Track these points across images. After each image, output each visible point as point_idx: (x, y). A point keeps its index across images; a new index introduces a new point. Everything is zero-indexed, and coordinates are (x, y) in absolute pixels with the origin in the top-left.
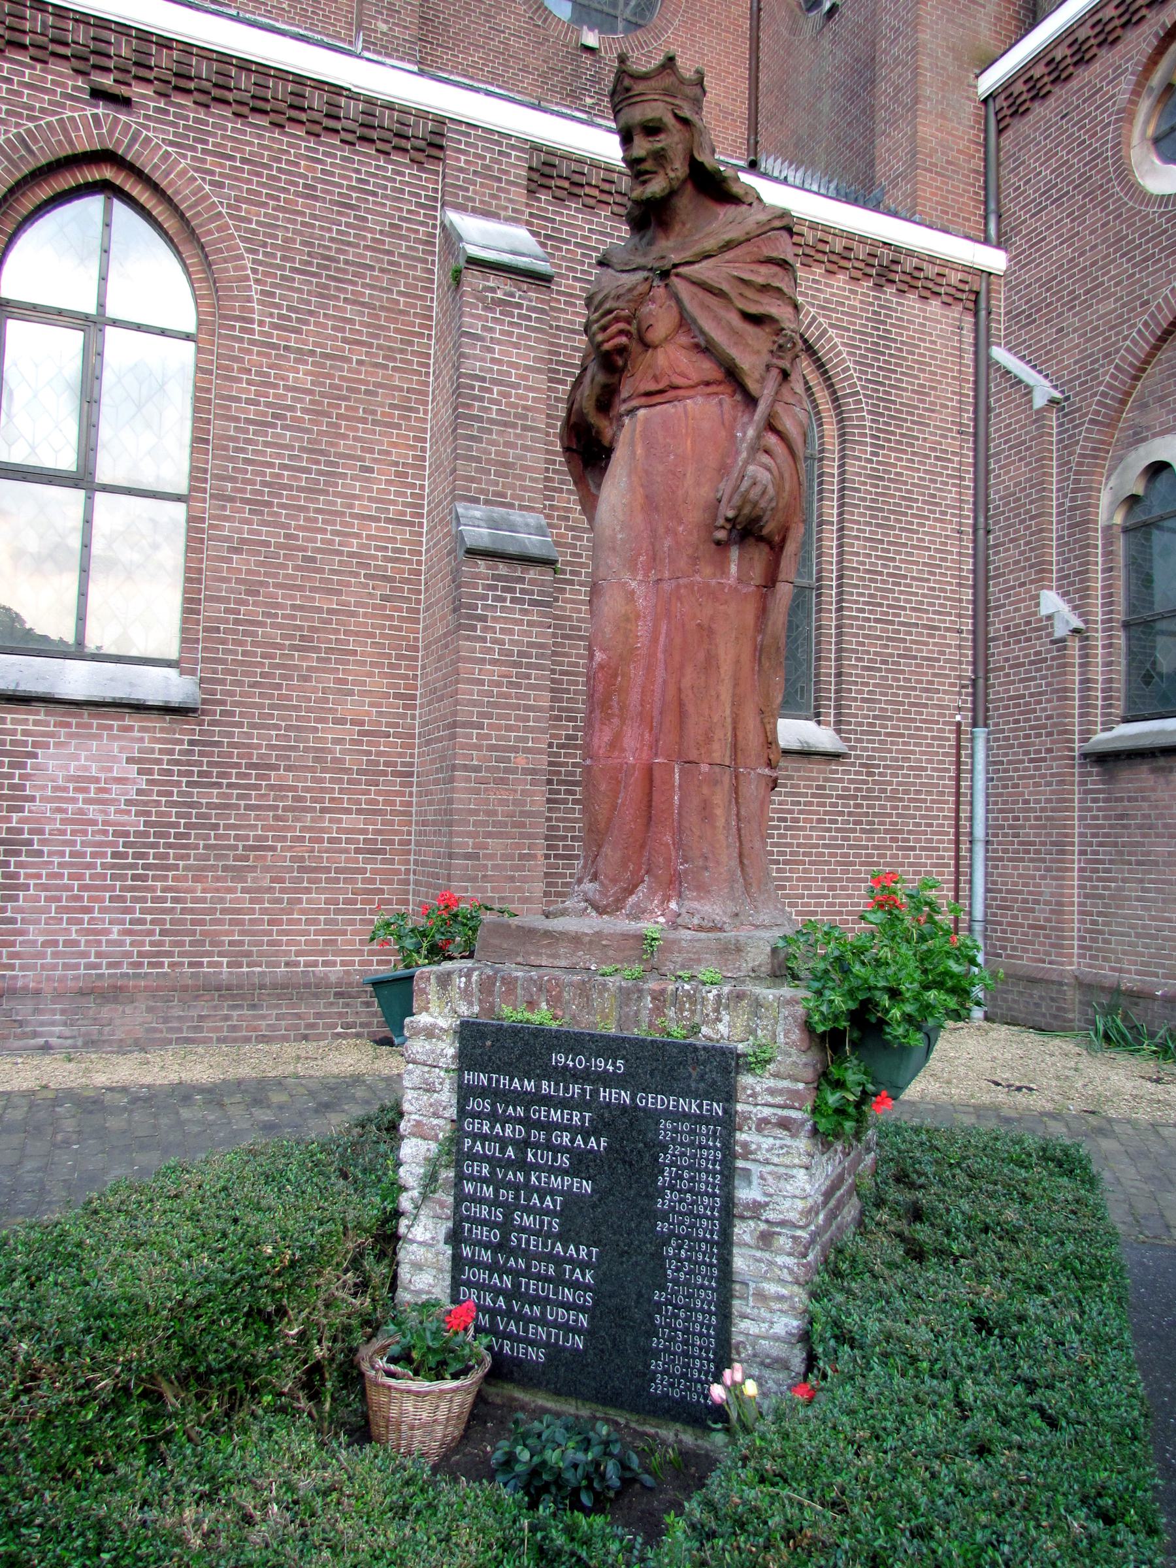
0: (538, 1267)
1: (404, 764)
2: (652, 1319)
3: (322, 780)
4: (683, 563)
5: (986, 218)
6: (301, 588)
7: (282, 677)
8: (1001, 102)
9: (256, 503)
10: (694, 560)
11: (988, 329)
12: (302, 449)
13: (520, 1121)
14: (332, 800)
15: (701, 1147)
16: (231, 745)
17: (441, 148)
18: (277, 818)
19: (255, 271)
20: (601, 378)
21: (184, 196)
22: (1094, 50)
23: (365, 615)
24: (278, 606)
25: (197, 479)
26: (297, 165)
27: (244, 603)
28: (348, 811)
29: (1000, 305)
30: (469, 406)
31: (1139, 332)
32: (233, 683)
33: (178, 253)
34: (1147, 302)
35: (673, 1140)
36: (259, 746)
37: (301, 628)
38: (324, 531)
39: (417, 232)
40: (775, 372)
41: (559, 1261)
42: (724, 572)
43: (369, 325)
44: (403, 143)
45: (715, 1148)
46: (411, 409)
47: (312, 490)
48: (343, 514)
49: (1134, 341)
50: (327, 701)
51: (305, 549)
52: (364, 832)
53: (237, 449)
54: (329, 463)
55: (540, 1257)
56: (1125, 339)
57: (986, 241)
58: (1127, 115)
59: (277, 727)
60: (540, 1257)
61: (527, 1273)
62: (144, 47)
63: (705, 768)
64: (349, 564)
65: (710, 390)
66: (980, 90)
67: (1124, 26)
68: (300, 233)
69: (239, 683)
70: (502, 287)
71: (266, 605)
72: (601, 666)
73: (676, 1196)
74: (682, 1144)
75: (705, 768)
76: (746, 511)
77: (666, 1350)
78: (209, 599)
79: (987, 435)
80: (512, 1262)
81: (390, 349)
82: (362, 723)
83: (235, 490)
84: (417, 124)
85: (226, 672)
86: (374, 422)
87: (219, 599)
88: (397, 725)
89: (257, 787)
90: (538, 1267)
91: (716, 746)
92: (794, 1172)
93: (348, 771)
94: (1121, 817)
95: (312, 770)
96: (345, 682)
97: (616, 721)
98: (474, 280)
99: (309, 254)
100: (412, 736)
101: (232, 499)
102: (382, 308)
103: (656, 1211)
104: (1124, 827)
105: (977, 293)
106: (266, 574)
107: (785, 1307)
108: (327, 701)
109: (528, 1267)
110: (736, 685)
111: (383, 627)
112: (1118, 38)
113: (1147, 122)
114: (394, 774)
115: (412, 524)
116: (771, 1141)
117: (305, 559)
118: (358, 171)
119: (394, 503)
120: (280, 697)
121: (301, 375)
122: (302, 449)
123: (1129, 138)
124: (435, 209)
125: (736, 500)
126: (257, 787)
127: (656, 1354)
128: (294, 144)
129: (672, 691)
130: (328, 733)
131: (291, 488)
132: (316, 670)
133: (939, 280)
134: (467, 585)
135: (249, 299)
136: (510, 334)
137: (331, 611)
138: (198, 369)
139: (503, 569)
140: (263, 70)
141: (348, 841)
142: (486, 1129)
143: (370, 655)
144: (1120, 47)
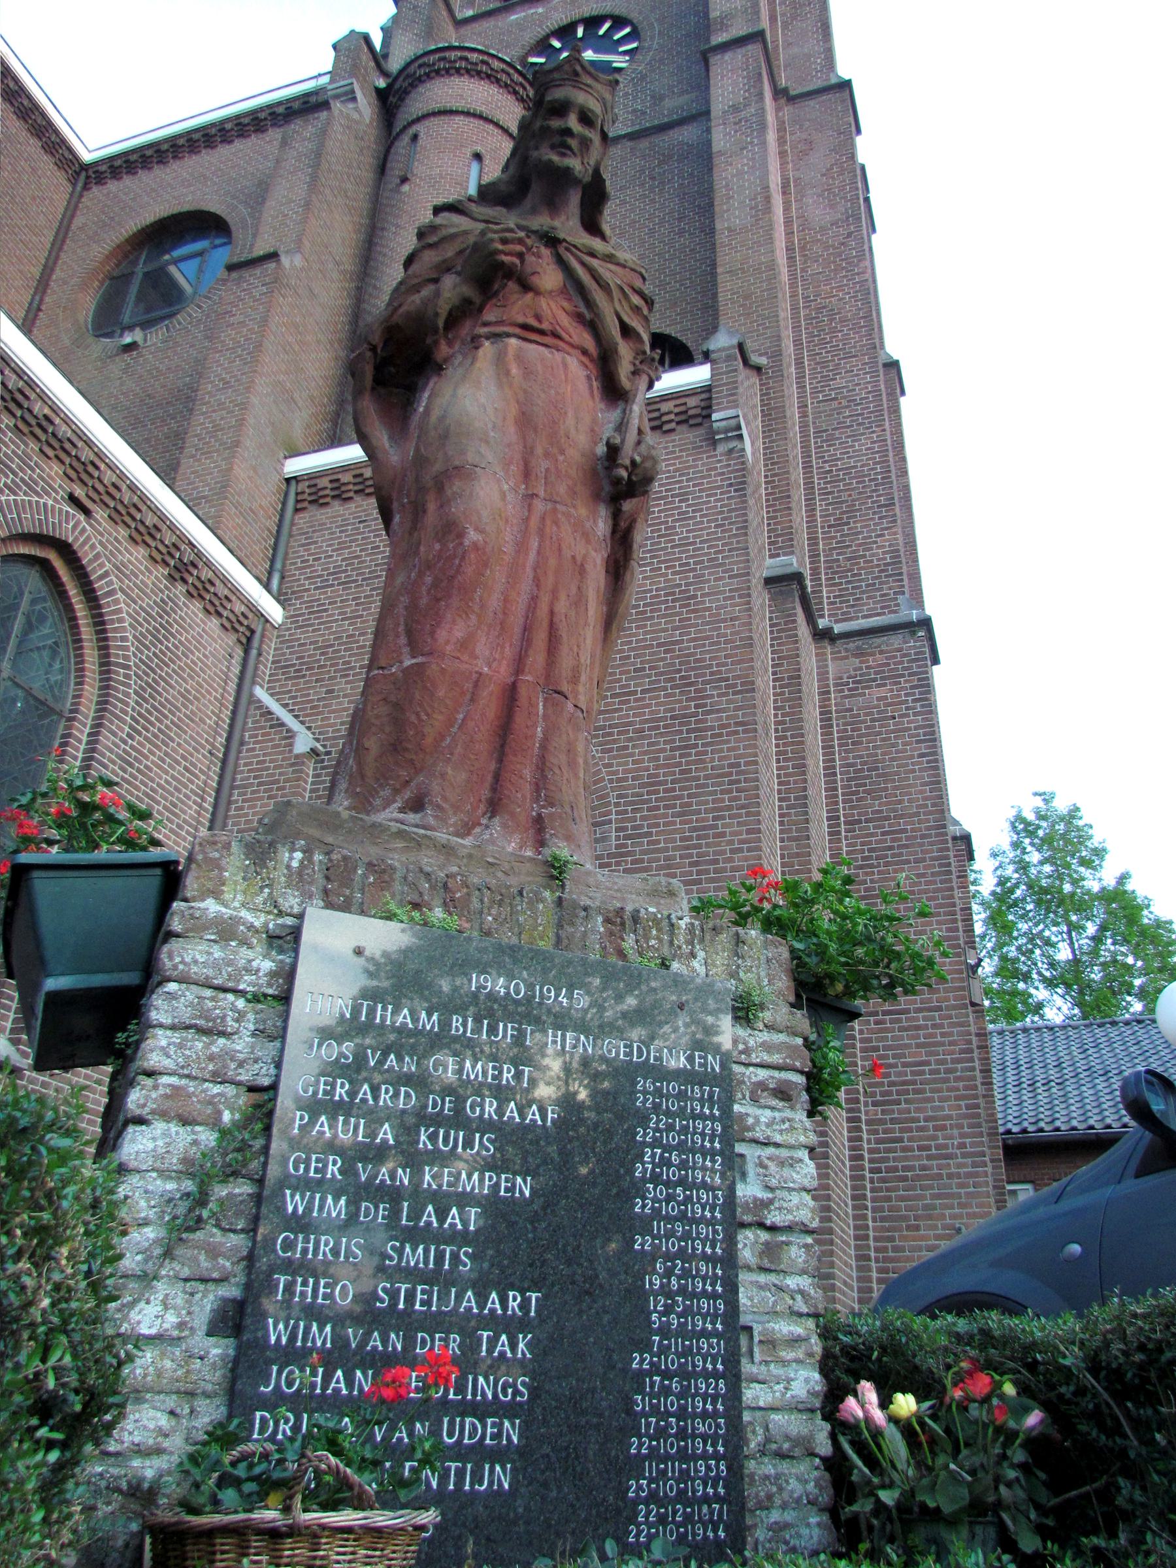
2: (629, 1403)
4: (562, 489)
8: (303, 486)
11: (256, 668)
13: (407, 1080)
15: (694, 1117)
29: (270, 655)
35: (656, 1107)
45: (712, 1117)
57: (267, 586)
65: (584, 359)
73: (662, 1192)
74: (668, 1113)
75: (570, 706)
79: (236, 765)
80: (376, 1341)
103: (633, 1217)
116: (768, 1113)
127: (635, 1466)
133: (225, 602)
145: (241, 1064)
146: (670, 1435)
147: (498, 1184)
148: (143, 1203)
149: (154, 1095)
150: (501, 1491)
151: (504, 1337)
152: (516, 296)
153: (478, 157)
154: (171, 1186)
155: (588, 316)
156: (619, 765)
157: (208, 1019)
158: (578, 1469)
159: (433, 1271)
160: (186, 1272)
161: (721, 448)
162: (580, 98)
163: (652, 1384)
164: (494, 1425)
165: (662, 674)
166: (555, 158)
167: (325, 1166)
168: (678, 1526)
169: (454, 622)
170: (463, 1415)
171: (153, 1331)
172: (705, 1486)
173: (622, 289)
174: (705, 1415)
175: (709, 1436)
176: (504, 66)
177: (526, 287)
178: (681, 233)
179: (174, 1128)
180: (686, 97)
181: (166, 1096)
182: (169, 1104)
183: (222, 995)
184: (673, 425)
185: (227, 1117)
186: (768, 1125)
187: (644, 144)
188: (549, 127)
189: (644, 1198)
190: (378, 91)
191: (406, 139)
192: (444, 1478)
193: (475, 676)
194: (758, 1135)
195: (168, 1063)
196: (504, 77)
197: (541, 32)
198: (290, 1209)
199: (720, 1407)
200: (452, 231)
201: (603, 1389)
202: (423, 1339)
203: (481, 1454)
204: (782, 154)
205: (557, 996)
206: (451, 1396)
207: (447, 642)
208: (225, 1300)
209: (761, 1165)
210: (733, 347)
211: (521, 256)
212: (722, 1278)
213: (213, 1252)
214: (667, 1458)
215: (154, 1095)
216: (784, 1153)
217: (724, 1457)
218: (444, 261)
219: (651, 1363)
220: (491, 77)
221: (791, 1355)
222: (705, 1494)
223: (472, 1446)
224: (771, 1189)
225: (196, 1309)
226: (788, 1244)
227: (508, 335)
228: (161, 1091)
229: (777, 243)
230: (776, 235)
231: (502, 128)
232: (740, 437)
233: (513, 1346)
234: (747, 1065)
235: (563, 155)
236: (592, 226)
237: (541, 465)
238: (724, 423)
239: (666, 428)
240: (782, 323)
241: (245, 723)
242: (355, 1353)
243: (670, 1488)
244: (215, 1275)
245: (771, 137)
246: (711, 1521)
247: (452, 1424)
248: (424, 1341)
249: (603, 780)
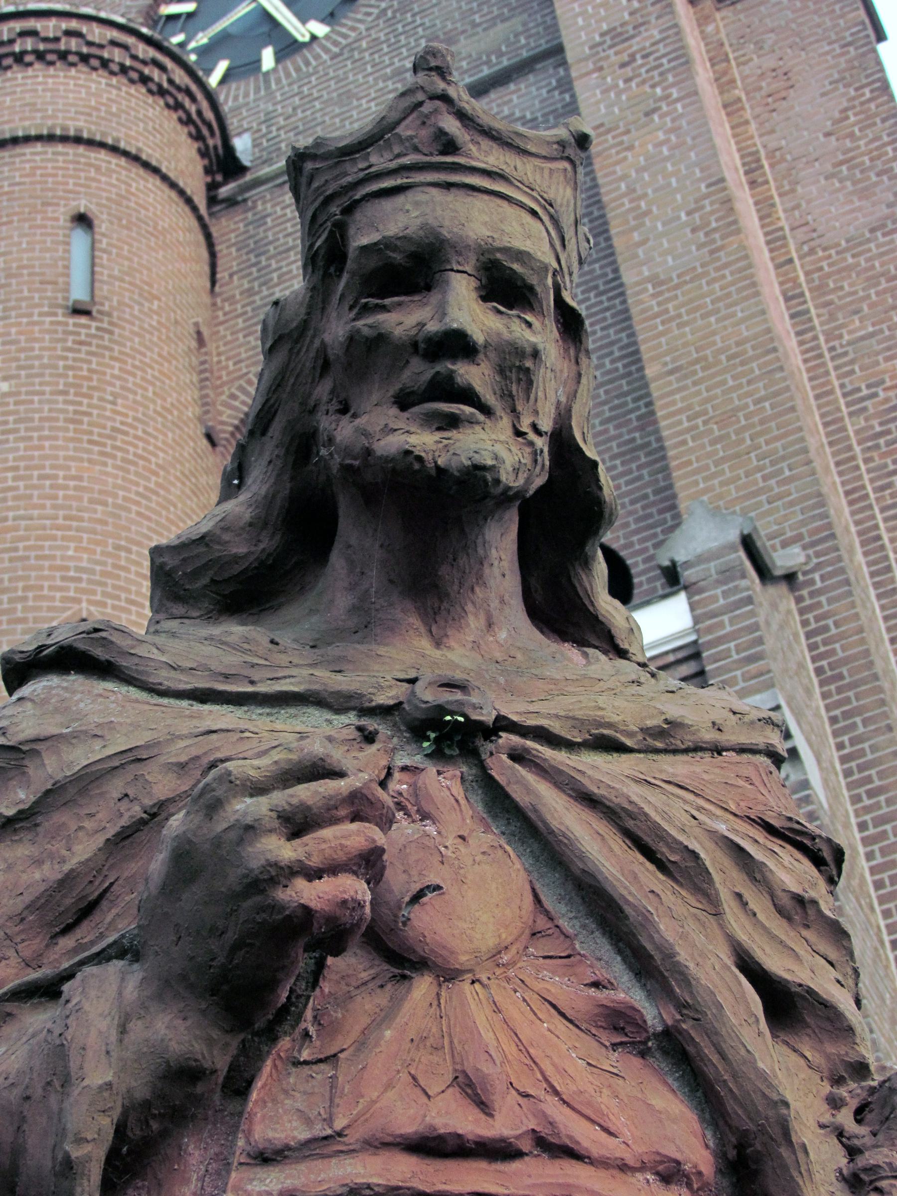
152: (368, 1004)
153: (83, 220)
155: (653, 1014)
162: (478, 221)
166: (424, 441)
173: (739, 853)
176: (115, 34)
177: (401, 958)
180: (501, 28)
188: (380, 339)
196: (117, 55)
200: (80, 757)
204: (731, 107)
210: (732, 548)
211: (370, 863)
218: (66, 882)
229: (765, 290)
230: (761, 276)
231: (125, 154)
235: (452, 422)
236: (562, 613)
240: (817, 464)
245: (703, 76)
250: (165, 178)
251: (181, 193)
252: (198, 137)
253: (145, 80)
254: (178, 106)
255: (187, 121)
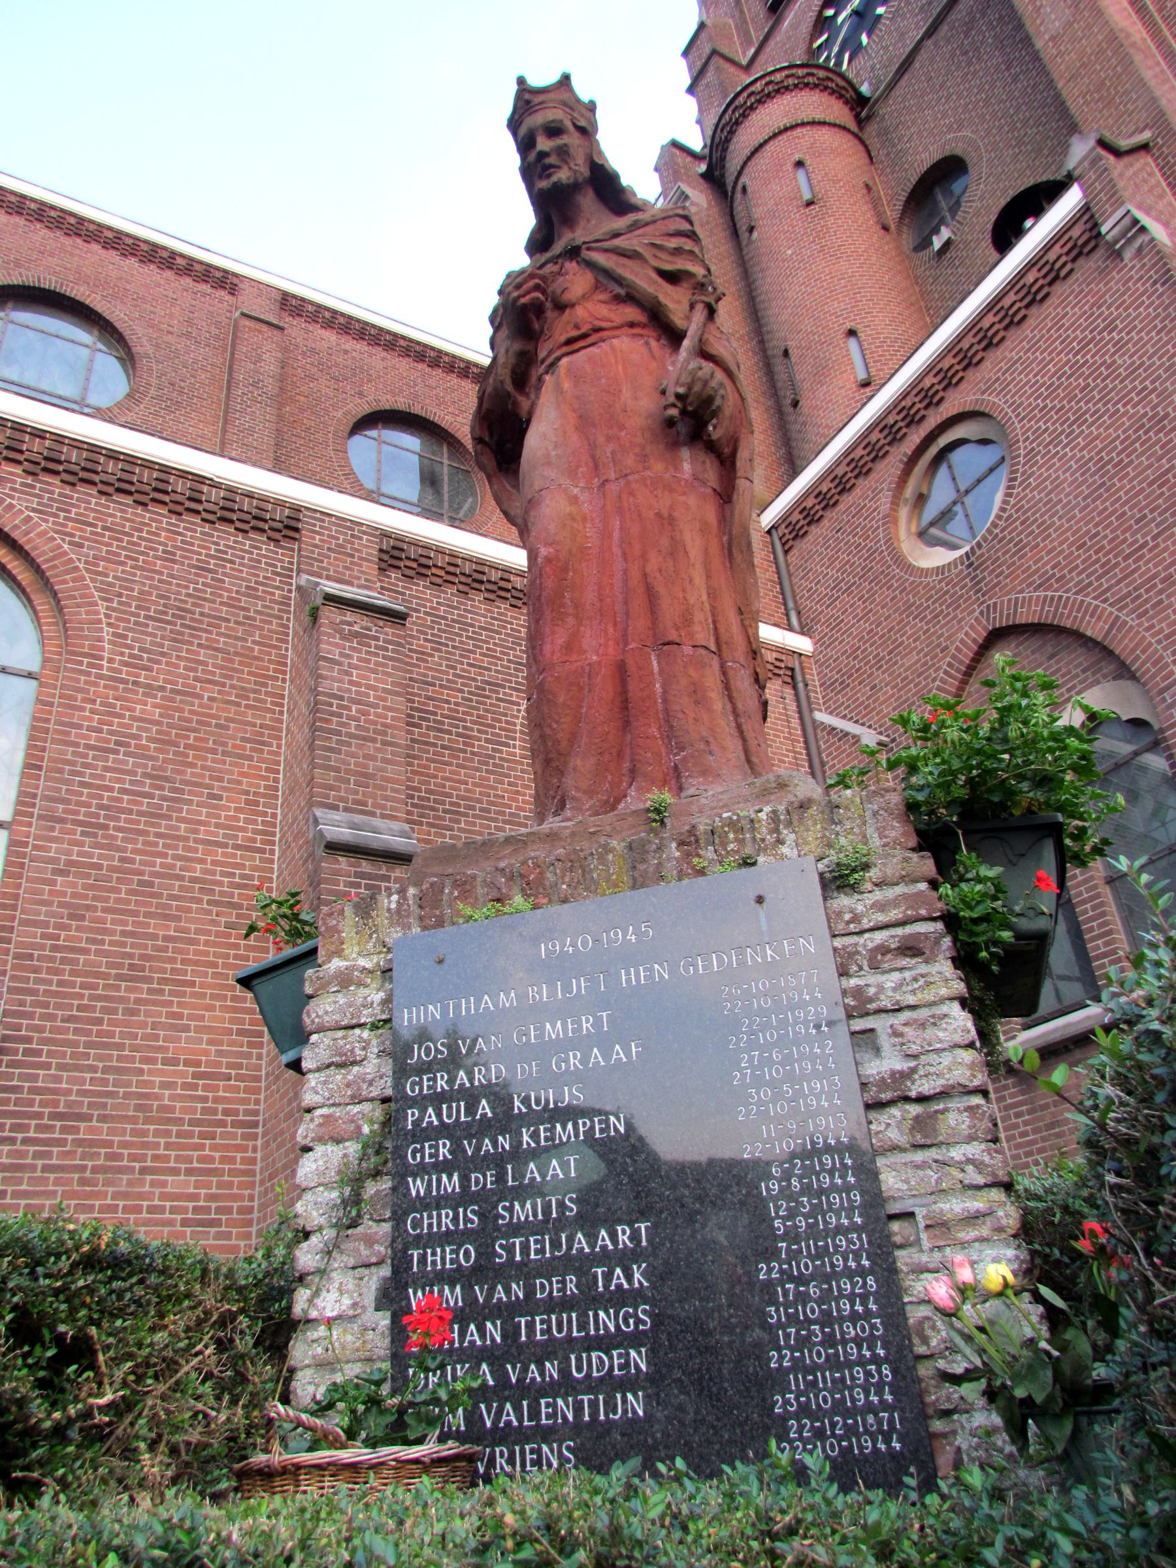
0: (547, 1288)
1: (247, 1112)
3: (145, 1133)
4: (630, 461)
5: (787, 615)
6: (134, 913)
7: (104, 1010)
9: (89, 825)
10: (643, 458)
11: (808, 698)
12: (145, 775)
14: (155, 1158)
16: (33, 1090)
17: (297, 530)
18: (83, 1182)
19: (108, 616)
20: (517, 346)
21: (41, 552)
22: (853, 481)
23: (207, 943)
24: (105, 931)
25: (27, 794)
26: (158, 535)
27: (66, 927)
28: (175, 1172)
29: (814, 680)
30: (327, 721)
31: (946, 672)
32: (43, 1017)
33: (29, 602)
34: (947, 647)
36: (69, 1092)
37: (131, 956)
38: (165, 855)
39: (273, 594)
40: (700, 307)
41: (580, 1265)
42: (677, 468)
43: (222, 667)
44: (261, 524)
46: (263, 743)
47: (154, 815)
48: (186, 839)
49: (942, 680)
50: (156, 1037)
51: (142, 873)
52: (194, 1197)
53: (72, 773)
54: (174, 790)
55: (547, 1269)
56: (934, 680)
57: (790, 629)
58: (891, 519)
59: (94, 1069)
60: (547, 1269)
61: (529, 1306)
62: (17, 435)
63: (687, 650)
64: (192, 890)
65: (635, 331)
66: (764, 524)
67: (873, 460)
68: (157, 588)
69: (51, 1018)
70: (359, 622)
71: (91, 930)
72: (548, 560)
73: (766, 1093)
75: (687, 650)
76: (697, 388)
77: (798, 1366)
78: (23, 922)
80: (500, 1293)
81: (243, 688)
82: (198, 1064)
83: (65, 811)
84: (275, 510)
85: (35, 1004)
86: (224, 753)
87: (35, 924)
88: (239, 1066)
89: (61, 1142)
90: (547, 1288)
91: (697, 628)
92: (944, 1009)
93: (179, 1121)
94: (1052, 1125)
95: (134, 1120)
96: (180, 1016)
97: (571, 620)
98: (330, 615)
99: (165, 606)
100: (258, 1079)
101: (62, 821)
102: (236, 654)
104: (1058, 1135)
105: (792, 670)
106: (95, 898)
107: (985, 1231)
108: (156, 1037)
109: (530, 1292)
110: (708, 577)
111: (227, 956)
112: (870, 470)
113: (909, 522)
114: (235, 1124)
115: (263, 851)
116: (896, 976)
117: (141, 883)
118: (217, 544)
119: (244, 830)
120: (100, 1034)
121: (151, 708)
122: (145, 775)
123: (897, 535)
124: (291, 577)
125: (685, 378)
126: (61, 1142)
127: (778, 1381)
128: (157, 519)
129: (635, 576)
130: (155, 1076)
131: (130, 812)
132: (145, 1002)
134: (327, 881)
135: (100, 639)
136: (368, 661)
137: (167, 939)
138: (39, 701)
139: (366, 866)
140: (131, 460)
141: (173, 1210)
142: (441, 1083)
143: (210, 986)
144: (873, 475)
145: (371, 1083)
146: (815, 1344)
147: (592, 1128)
148: (315, 1213)
149: (312, 1126)
150: (636, 1419)
151: (618, 1271)
154: (335, 1194)
155: (622, 292)
156: (1160, 622)
157: (341, 1055)
158: (714, 1389)
159: (543, 1221)
160: (352, 1262)
161: (1128, 255)
163: (786, 1293)
164: (620, 1356)
165: (1166, 510)
167: (437, 1150)
168: (840, 1439)
169: (553, 633)
170: (588, 1350)
171: (335, 1313)
172: (867, 1394)
173: (653, 245)
174: (854, 1317)
175: (863, 1340)
176: (786, 72)
178: (1015, 79)
179: (330, 1148)
181: (320, 1125)
182: (323, 1129)
183: (351, 1032)
184: (1068, 267)
185: (366, 1129)
186: (895, 989)
187: (944, 29)
189: (747, 1104)
190: (703, 176)
191: (738, 195)
192: (578, 1409)
193: (587, 669)
194: (886, 1003)
195: (317, 1099)
196: (791, 81)
197: (812, 15)
198: (414, 1193)
199: (873, 1307)
201: (730, 1306)
202: (542, 1285)
203: (612, 1385)
205: (624, 935)
206: (575, 1334)
207: (553, 653)
208: (385, 1279)
209: (896, 1034)
210: (1093, 149)
212: (853, 1168)
213: (370, 1241)
214: (814, 1369)
215: (312, 1126)
216: (923, 1013)
217: (886, 1360)
219: (781, 1271)
220: (782, 90)
221: (973, 1234)
222: (868, 1402)
223: (602, 1379)
224: (915, 1057)
225: (364, 1290)
226: (946, 1110)
227: (559, 359)
228: (317, 1121)
231: (808, 123)
232: (1143, 229)
233: (629, 1277)
234: (861, 933)
235: (550, 176)
237: (607, 450)
238: (1117, 229)
239: (1063, 273)
241: (818, 747)
242: (484, 1307)
243: (825, 1399)
244: (374, 1260)
246: (882, 1432)
247: (579, 1360)
248: (542, 1286)
249: (1150, 644)
250: (829, 124)
251: (840, 127)
252: (841, 96)
253: (807, 85)
254: (826, 88)
255: (833, 92)
